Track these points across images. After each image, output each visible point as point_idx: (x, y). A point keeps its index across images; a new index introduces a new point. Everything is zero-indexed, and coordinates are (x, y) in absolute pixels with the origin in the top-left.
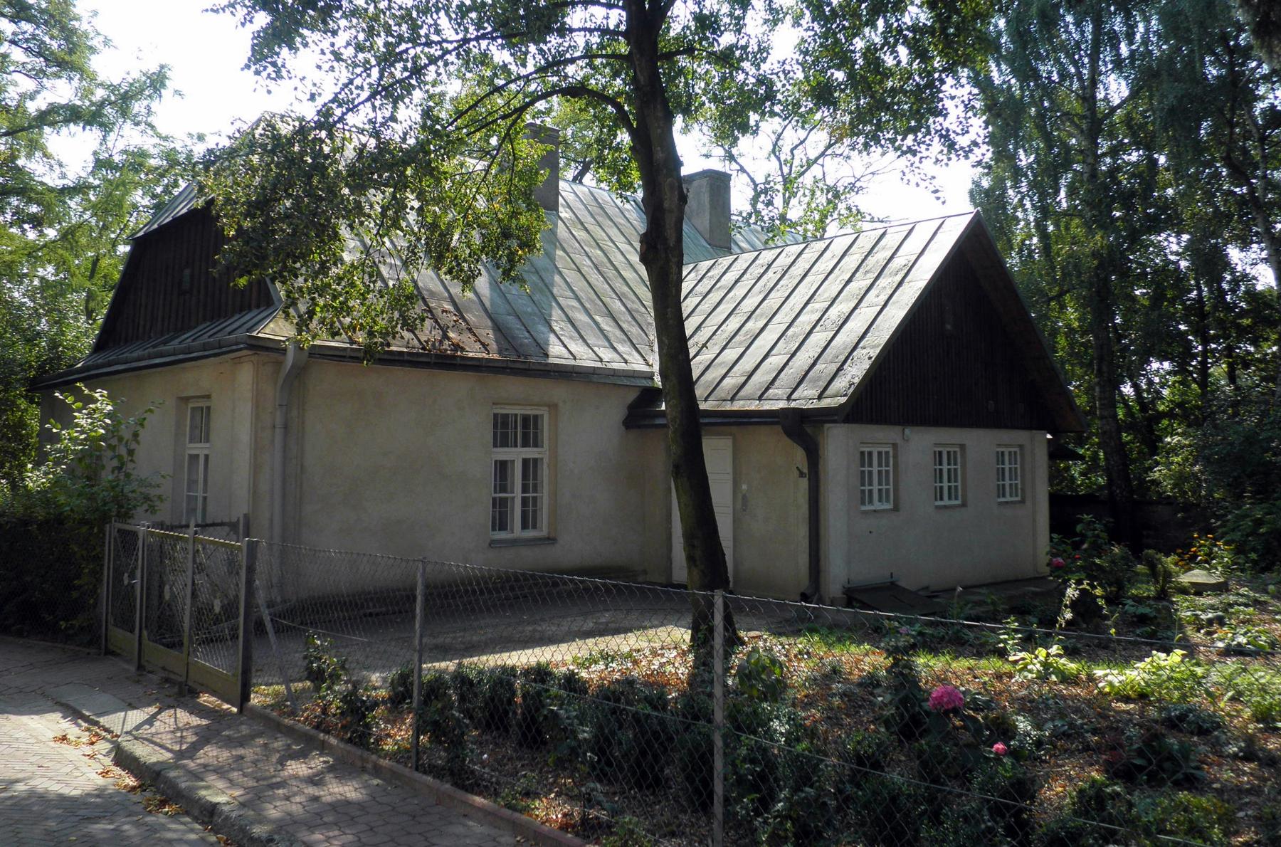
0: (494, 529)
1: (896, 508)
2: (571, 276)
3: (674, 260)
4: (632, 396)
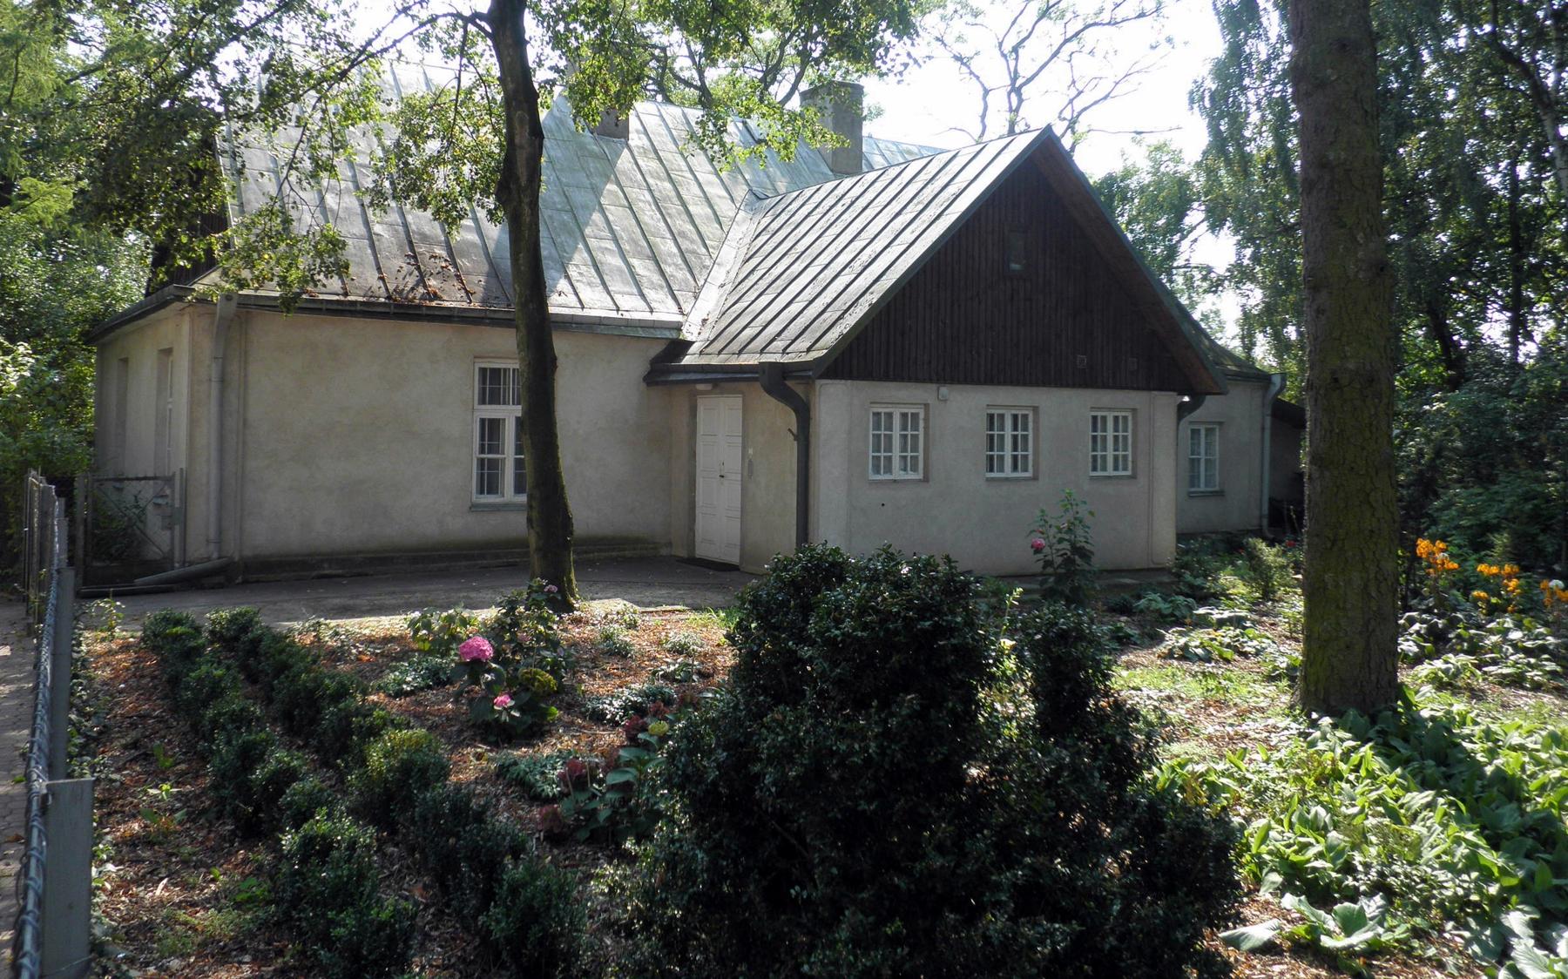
0: (481, 492)
1: (926, 479)
2: (616, 214)
3: (526, 200)
4: (656, 350)
